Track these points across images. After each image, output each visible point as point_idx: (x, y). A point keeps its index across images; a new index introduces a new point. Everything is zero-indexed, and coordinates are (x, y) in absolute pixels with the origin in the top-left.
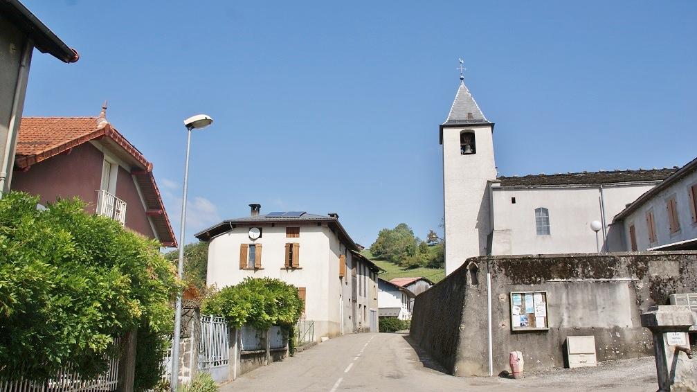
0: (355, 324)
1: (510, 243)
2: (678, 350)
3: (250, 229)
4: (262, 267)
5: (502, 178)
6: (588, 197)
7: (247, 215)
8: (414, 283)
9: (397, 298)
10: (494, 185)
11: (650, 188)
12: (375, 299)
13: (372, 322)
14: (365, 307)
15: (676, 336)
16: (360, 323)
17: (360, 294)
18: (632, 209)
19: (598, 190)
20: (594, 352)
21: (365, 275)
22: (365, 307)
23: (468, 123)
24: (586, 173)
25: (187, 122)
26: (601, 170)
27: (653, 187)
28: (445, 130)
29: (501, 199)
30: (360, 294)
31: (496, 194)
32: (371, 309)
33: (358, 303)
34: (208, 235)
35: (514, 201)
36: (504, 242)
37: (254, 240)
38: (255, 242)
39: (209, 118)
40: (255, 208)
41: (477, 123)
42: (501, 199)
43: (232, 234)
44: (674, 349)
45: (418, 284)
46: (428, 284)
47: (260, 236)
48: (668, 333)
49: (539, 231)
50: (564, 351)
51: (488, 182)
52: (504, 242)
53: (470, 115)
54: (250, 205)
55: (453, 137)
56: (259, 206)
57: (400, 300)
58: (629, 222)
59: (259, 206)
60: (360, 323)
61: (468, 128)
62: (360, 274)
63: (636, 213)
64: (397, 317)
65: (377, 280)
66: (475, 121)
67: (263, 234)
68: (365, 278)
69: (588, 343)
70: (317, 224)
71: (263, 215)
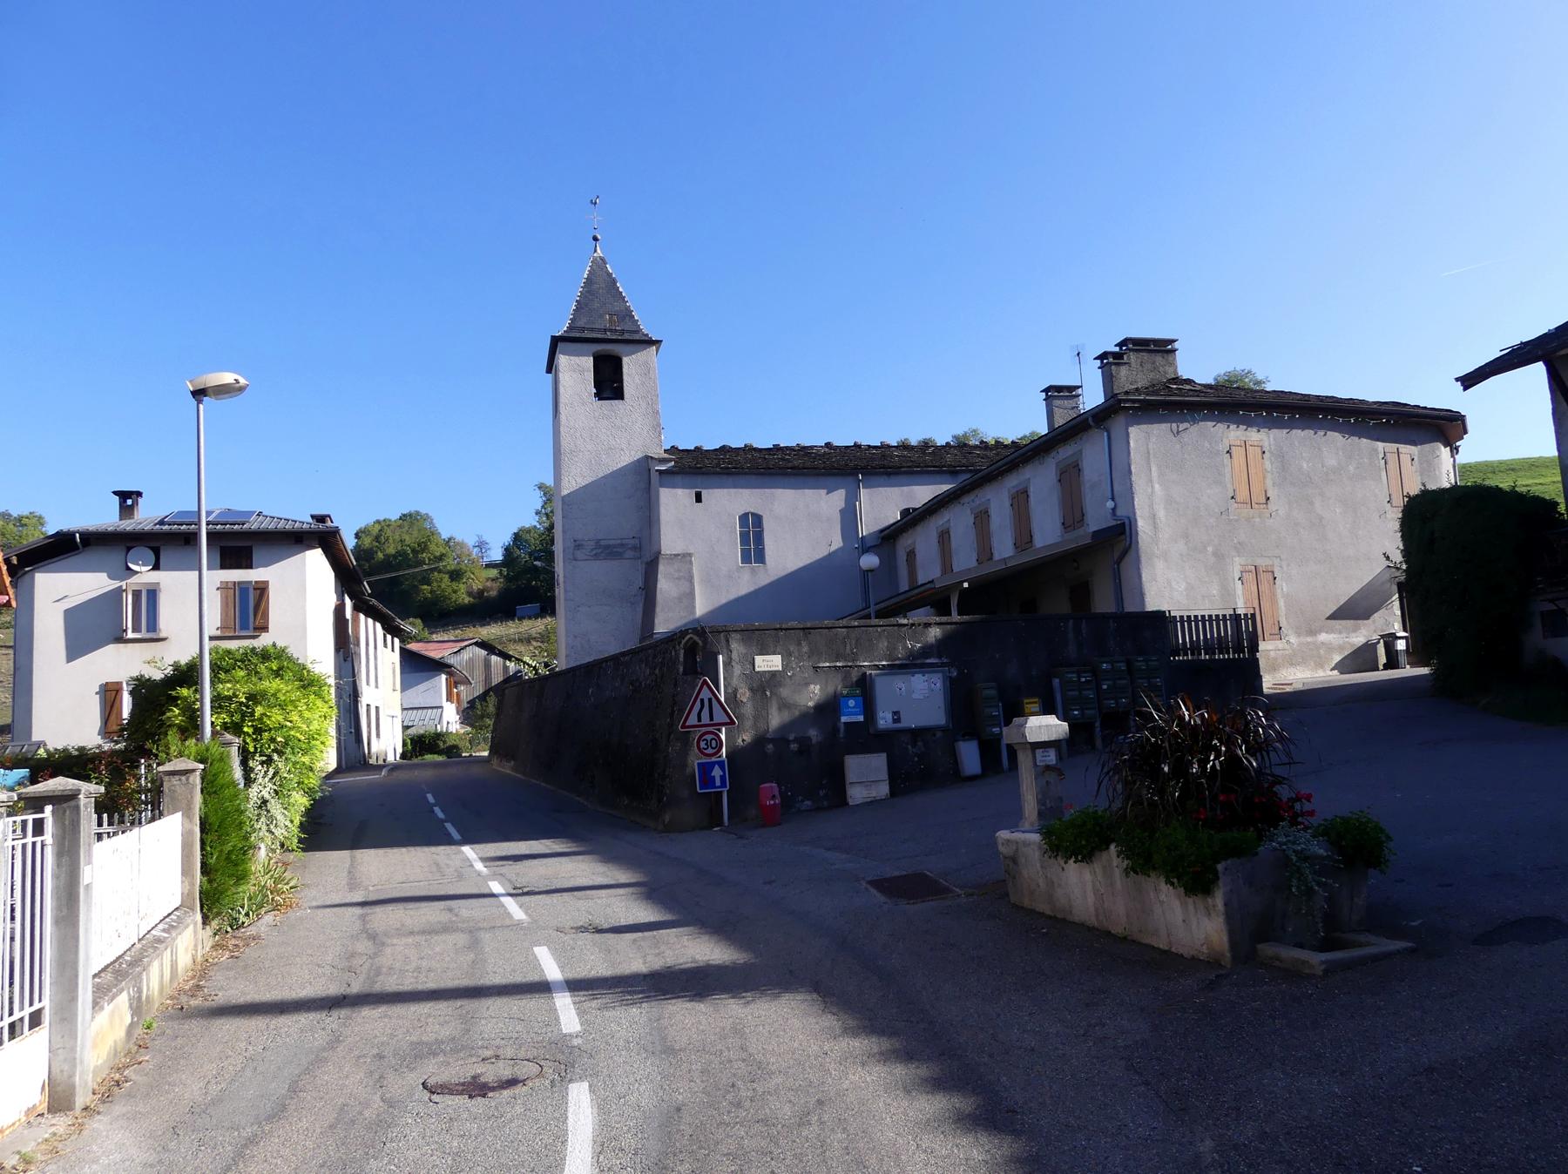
3: (129, 549)
4: (162, 635)
7: (107, 517)
11: (945, 487)
18: (912, 519)
23: (609, 335)
39: (243, 381)
40: (128, 500)
49: (746, 558)
58: (905, 542)
63: (919, 528)
69: (877, 764)
71: (147, 515)
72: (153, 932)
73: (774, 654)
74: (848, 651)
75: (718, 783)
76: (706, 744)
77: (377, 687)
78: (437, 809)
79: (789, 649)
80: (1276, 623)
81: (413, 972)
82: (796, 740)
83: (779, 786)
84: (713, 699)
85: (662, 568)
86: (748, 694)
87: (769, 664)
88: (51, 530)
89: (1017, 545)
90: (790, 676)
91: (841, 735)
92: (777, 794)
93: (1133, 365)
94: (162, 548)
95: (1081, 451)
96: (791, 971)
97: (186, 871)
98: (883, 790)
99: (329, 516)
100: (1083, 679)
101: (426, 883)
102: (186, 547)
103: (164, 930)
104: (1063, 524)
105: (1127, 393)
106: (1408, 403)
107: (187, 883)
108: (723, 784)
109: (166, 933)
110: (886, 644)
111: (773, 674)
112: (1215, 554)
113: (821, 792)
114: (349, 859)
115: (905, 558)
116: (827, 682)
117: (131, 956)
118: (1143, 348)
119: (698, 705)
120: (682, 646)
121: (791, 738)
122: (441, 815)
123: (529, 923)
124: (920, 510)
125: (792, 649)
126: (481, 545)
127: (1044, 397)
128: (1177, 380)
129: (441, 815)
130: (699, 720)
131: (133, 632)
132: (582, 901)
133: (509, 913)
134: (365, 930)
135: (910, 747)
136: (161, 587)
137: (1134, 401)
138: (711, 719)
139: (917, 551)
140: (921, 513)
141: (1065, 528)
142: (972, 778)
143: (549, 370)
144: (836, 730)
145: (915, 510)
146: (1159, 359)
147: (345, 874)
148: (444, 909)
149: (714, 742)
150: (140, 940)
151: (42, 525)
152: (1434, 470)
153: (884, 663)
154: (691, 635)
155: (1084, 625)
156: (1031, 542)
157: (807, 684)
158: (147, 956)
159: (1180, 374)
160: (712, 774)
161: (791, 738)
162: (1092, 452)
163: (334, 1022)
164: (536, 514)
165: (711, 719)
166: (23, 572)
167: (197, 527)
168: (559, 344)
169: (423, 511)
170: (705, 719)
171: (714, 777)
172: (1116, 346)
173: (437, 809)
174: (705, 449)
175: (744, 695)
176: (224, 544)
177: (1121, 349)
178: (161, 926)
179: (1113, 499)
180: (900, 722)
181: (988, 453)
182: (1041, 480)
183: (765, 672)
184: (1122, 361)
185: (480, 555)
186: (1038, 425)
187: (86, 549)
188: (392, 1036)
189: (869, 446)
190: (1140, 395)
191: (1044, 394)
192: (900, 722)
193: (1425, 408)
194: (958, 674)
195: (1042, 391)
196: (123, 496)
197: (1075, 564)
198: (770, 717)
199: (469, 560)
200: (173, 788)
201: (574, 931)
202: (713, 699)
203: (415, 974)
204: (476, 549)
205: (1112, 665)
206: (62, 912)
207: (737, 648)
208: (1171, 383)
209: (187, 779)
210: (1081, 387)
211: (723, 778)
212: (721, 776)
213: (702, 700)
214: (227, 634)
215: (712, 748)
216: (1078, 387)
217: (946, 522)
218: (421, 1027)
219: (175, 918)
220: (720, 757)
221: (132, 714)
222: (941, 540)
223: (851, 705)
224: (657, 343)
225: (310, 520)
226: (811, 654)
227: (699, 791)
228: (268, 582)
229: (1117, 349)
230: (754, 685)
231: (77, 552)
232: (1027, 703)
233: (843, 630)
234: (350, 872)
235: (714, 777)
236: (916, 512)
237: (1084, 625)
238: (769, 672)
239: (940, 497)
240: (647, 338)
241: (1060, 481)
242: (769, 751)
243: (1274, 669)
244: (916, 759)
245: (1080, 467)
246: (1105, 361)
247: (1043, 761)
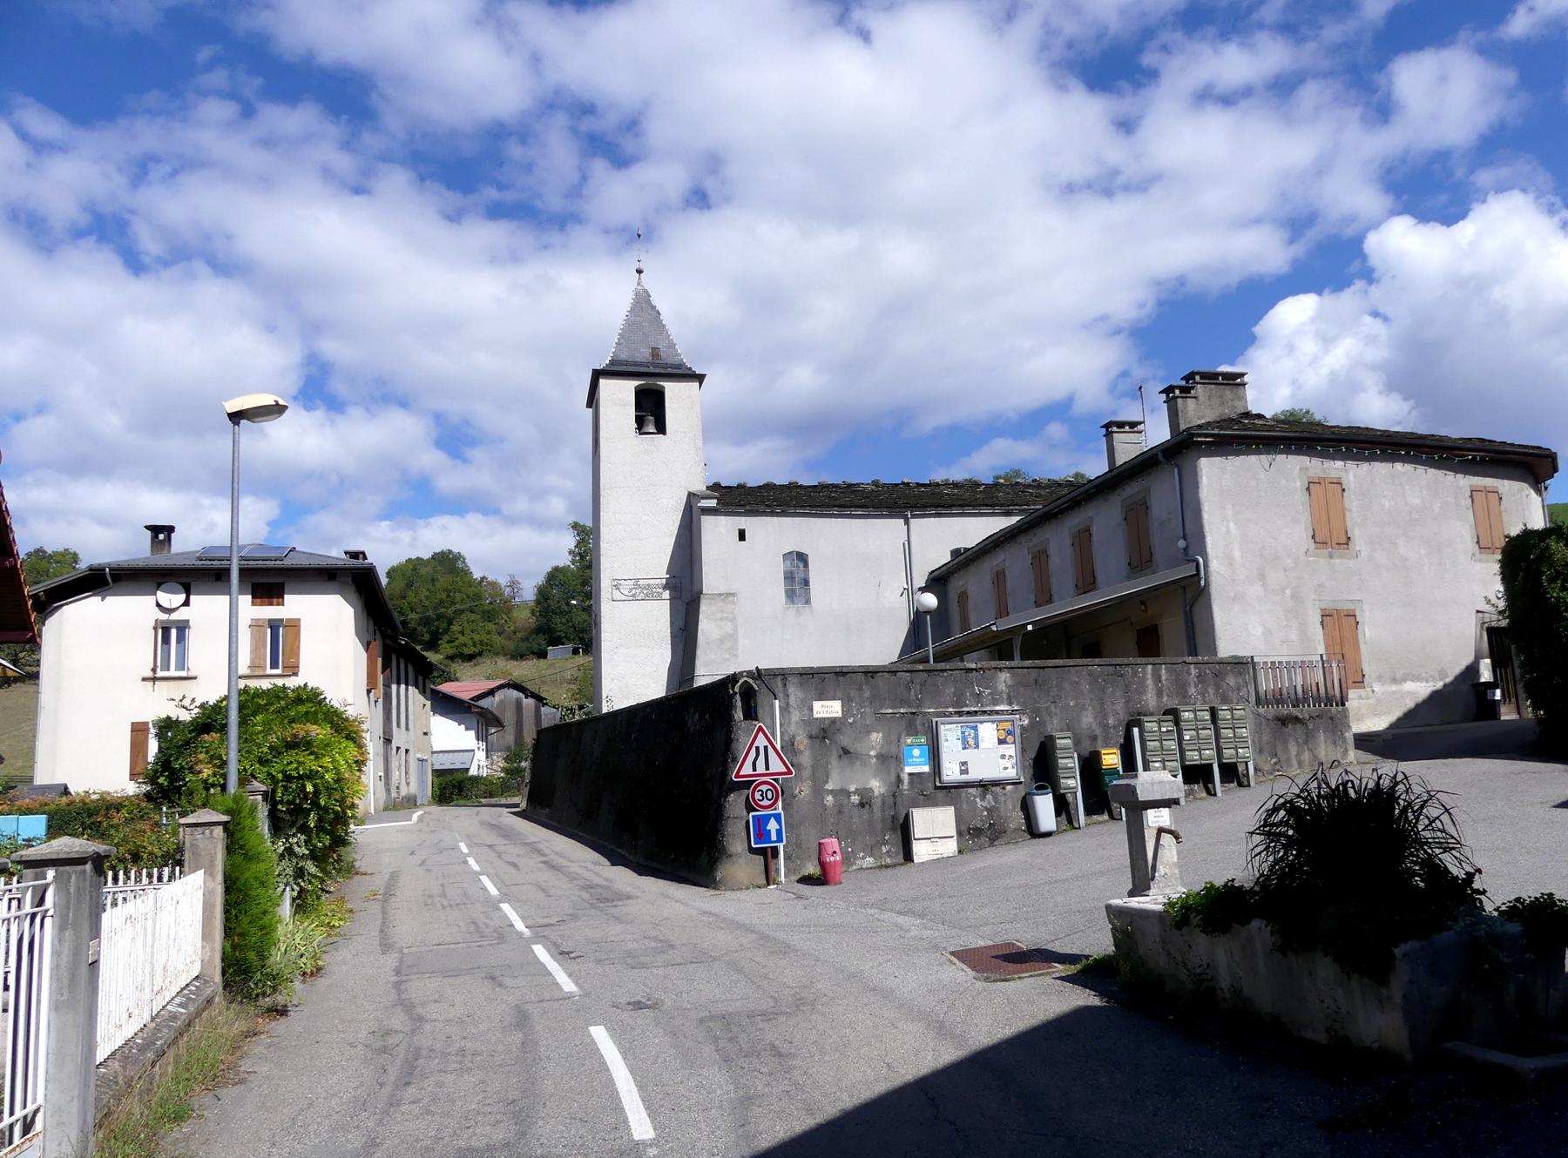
0: (388, 791)
1: (733, 620)
2: (1161, 831)
4: (192, 674)
5: (716, 487)
6: (884, 533)
7: (136, 549)
8: (491, 692)
9: (467, 729)
10: (705, 503)
11: (1014, 520)
12: (425, 734)
13: (417, 783)
14: (407, 751)
15: (1159, 814)
16: (398, 788)
17: (398, 726)
18: (964, 560)
19: (902, 521)
20: (954, 834)
21: (407, 685)
22: (407, 751)
23: (652, 370)
24: (876, 483)
25: (234, 406)
26: (906, 481)
27: (1019, 518)
28: (603, 382)
29: (717, 531)
30: (398, 726)
31: (708, 523)
32: (419, 756)
33: (394, 745)
34: (43, 598)
35: (742, 535)
36: (721, 619)
37: (169, 611)
38: (174, 616)
39: (281, 402)
41: (670, 371)
42: (717, 531)
43: (109, 599)
44: (1156, 832)
45: (499, 696)
46: (521, 695)
47: (186, 603)
48: (1148, 811)
49: (791, 595)
50: (905, 833)
51: (690, 494)
52: (721, 619)
53: (655, 352)
54: (148, 527)
55: (620, 395)
56: (169, 530)
57: (472, 734)
59: (169, 530)
60: (398, 788)
61: (651, 381)
62: (399, 683)
63: (972, 569)
64: (467, 770)
65: (428, 691)
66: (666, 366)
67: (192, 597)
68: (407, 690)
70: (321, 577)
72: (169, 1007)
73: (834, 699)
74: (913, 697)
75: (774, 838)
76: (762, 795)
77: (407, 729)
78: (471, 861)
79: (849, 694)
80: (1359, 671)
81: (457, 1055)
82: (857, 792)
83: (840, 844)
84: (770, 748)
85: (704, 607)
86: (806, 741)
87: (829, 710)
88: (83, 565)
89: (1079, 586)
90: (851, 724)
91: (905, 788)
92: (838, 851)
93: (1201, 398)
94: (192, 583)
95: (1148, 490)
96: (888, 1064)
97: (206, 936)
98: (950, 847)
99: (363, 553)
100: (1164, 729)
101: (464, 945)
102: (219, 583)
103: (180, 1005)
104: (1129, 564)
105: (1200, 426)
106: (1494, 439)
107: (207, 949)
108: (780, 839)
109: (183, 1008)
110: (952, 690)
111: (833, 721)
112: (1293, 597)
113: (883, 848)
114: (381, 916)
115: (957, 600)
116: (890, 729)
117: (143, 1039)
118: (1213, 381)
119: (753, 753)
120: (737, 690)
121: (852, 789)
122: (476, 867)
123: (580, 996)
124: (974, 550)
125: (852, 694)
126: (513, 584)
127: (1104, 433)
128: (1247, 415)
129: (476, 867)
130: (754, 769)
131: (271, 668)
132: (637, 971)
133: (557, 984)
134: (401, 1002)
135: (978, 800)
136: (190, 623)
137: (1206, 436)
138: (767, 768)
139: (968, 591)
140: (974, 553)
141: (1132, 568)
142: (1048, 834)
143: (589, 405)
144: (899, 780)
145: (967, 550)
146: (1228, 393)
147: (377, 933)
148: (486, 978)
149: (769, 793)
150: (153, 1019)
151: (76, 562)
152: (1524, 510)
153: (951, 710)
154: (746, 679)
155: (1163, 672)
156: (1094, 582)
157: (869, 732)
158: (161, 1038)
159: (1249, 409)
160: (768, 828)
161: (852, 789)
162: (1160, 491)
163: (368, 1119)
164: (570, 553)
165: (767, 768)
166: (52, 608)
167: (228, 562)
168: (601, 381)
169: (455, 550)
170: (761, 768)
171: (770, 831)
172: (1182, 379)
173: (471, 861)
174: (748, 485)
175: (802, 741)
176: (256, 580)
177: (1187, 382)
178: (177, 1000)
179: (1185, 538)
180: (967, 773)
181: (1042, 492)
182: (1105, 520)
183: (825, 718)
184: (1189, 395)
185: (512, 594)
186: (1095, 467)
187: (117, 584)
188: (437, 1139)
189: (917, 484)
190: (1213, 429)
191: (1104, 429)
192: (967, 773)
193: (1513, 444)
194: (1030, 722)
195: (1102, 427)
196: (155, 530)
197: (1143, 607)
198: (830, 766)
199: (500, 600)
200: (195, 842)
201: (631, 1007)
202: (770, 748)
203: (459, 1058)
204: (507, 589)
205: (1195, 714)
206: (62, 995)
207: (795, 692)
208: (1242, 418)
209: (211, 833)
210: (1144, 422)
211: (779, 832)
212: (777, 830)
213: (757, 748)
214: (257, 673)
215: (768, 799)
216: (1140, 423)
217: (1001, 562)
218: (468, 1128)
219: (194, 988)
220: (775, 809)
221: (157, 758)
222: (996, 582)
223: (915, 755)
224: (700, 378)
225: (344, 556)
226: (872, 700)
227: (754, 846)
228: (299, 620)
229: (1183, 383)
230: (813, 732)
231: (107, 587)
232: (1104, 754)
233: (907, 674)
234: (382, 931)
235: (770, 831)
236: (969, 552)
237: (1163, 672)
238: (828, 718)
239: (993, 538)
240: (690, 372)
241: (1125, 519)
242: (828, 804)
243: (1360, 719)
244: (985, 813)
245: (1148, 504)
246: (1171, 395)
247: (1155, 822)
